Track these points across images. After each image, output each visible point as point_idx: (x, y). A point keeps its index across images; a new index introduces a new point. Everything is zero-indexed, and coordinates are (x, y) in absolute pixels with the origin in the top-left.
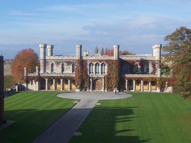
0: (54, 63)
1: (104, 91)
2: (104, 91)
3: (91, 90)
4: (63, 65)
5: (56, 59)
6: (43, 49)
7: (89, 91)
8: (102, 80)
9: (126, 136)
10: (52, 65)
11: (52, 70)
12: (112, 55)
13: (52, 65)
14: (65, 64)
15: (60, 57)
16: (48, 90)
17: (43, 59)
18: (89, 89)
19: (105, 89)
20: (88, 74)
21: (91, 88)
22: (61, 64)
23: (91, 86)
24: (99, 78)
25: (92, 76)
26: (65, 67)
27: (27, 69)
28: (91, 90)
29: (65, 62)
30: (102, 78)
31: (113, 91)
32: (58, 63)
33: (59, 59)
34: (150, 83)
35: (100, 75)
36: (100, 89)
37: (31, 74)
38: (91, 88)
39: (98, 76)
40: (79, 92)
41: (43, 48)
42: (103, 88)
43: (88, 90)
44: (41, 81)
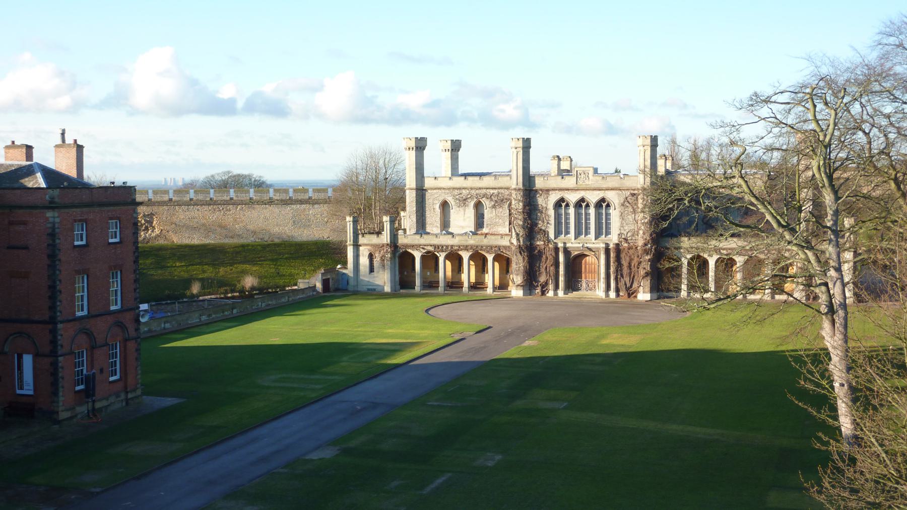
0: (450, 200)
1: (607, 295)
2: (607, 295)
3: (561, 293)
4: (478, 206)
5: (458, 186)
6: (413, 153)
7: (556, 294)
8: (598, 259)
9: (197, 246)
10: (445, 205)
11: (445, 224)
12: (22, 388)
13: (445, 205)
14: (486, 203)
15: (470, 178)
16: (689, 293)
17: (414, 185)
18: (557, 287)
19: (608, 288)
20: (552, 236)
21: (562, 284)
22: (472, 204)
23: (562, 279)
24: (590, 249)
25: (565, 243)
26: (488, 214)
27: (355, 222)
28: (561, 293)
29: (485, 196)
30: (598, 249)
31: (636, 297)
32: (464, 201)
33: (465, 186)
34: (466, 285)
35: (590, 240)
36: (593, 288)
37: (367, 236)
38: (562, 284)
39: (586, 245)
40: (518, 300)
41: (414, 152)
42: (602, 285)
43: (551, 294)
44: (869, 101)
